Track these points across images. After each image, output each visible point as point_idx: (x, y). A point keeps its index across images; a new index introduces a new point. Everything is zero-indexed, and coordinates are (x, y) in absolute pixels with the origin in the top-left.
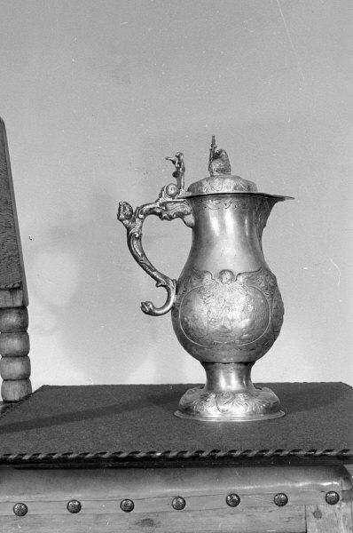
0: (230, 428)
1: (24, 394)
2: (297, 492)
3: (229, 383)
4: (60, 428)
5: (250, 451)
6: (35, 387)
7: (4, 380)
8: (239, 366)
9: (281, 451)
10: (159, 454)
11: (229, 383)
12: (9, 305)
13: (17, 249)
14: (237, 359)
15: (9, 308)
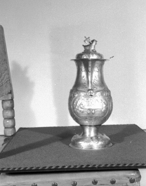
0: (90, 152)
1: (13, 134)
2: (119, 179)
3: (90, 132)
4: (28, 153)
5: (101, 165)
6: (17, 128)
7: (5, 128)
8: (98, 134)
9: (113, 165)
10: (66, 167)
11: (90, 132)
12: (7, 99)
13: (9, 77)
14: (95, 124)
15: (7, 100)
